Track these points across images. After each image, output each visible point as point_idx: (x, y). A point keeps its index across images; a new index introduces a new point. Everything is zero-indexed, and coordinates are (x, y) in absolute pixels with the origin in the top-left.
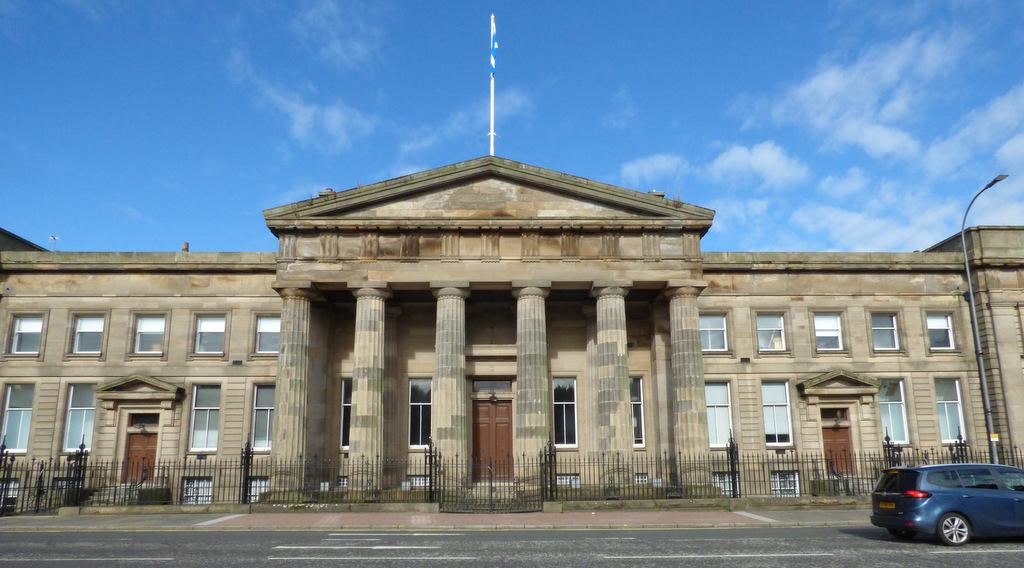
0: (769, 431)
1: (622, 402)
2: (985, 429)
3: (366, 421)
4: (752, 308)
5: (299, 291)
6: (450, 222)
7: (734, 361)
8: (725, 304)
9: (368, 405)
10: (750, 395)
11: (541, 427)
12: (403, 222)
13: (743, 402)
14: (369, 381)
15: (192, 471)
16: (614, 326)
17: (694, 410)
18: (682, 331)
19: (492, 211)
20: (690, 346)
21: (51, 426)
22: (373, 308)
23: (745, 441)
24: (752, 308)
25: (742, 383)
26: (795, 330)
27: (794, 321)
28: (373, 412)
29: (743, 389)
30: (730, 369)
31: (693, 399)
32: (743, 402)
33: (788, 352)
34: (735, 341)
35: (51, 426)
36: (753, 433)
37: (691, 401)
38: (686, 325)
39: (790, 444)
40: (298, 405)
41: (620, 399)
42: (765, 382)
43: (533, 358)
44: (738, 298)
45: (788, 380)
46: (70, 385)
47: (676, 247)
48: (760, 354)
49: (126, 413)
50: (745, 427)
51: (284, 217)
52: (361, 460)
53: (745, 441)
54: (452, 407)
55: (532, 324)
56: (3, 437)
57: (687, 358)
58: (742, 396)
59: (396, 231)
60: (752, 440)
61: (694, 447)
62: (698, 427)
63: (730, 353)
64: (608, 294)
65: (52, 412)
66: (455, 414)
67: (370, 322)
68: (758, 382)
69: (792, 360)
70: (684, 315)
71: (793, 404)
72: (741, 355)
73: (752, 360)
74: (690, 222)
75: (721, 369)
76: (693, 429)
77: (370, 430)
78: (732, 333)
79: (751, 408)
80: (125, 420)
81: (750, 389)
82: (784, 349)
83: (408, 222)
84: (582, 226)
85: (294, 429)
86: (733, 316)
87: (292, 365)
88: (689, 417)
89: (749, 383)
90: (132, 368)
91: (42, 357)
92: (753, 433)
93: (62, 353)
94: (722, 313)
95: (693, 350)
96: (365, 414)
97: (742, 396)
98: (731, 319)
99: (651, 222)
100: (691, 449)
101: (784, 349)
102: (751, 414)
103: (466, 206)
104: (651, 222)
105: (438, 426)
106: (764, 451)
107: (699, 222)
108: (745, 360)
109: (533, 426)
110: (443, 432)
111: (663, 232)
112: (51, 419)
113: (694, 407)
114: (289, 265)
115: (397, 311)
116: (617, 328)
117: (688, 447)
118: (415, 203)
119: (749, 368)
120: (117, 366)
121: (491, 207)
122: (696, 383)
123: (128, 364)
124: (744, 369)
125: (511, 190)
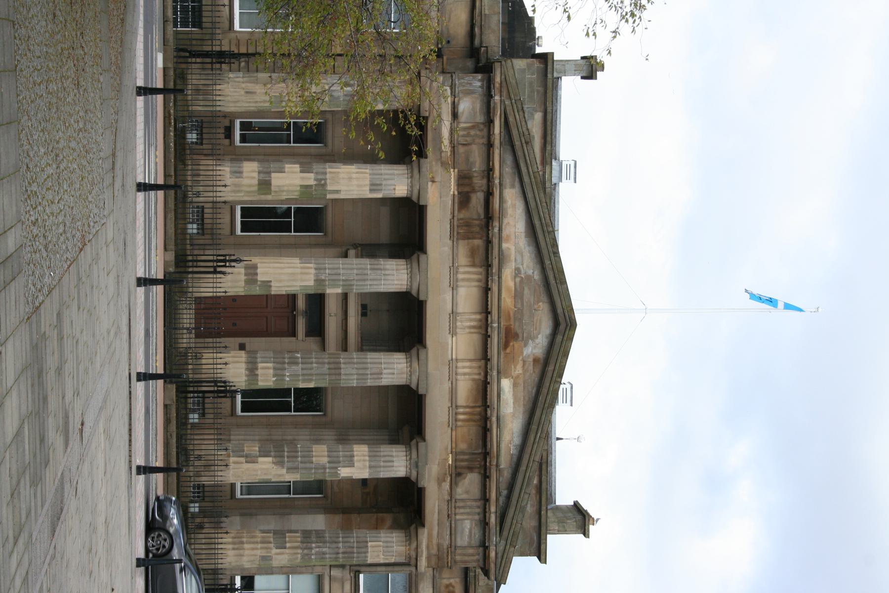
1: (284, 471)
14: (311, 186)
15: (209, 20)
16: (373, 464)
17: (275, 551)
18: (367, 542)
20: (349, 550)
31: (287, 551)
37: (285, 548)
38: (372, 547)
41: (288, 469)
47: (466, 538)
51: (504, 84)
57: (334, 545)
64: (410, 459)
85: (256, 102)
103: (518, 295)
105: (259, 265)
110: (252, 271)
113: (278, 551)
114: (448, 89)
118: (523, 235)
121: (517, 324)
122: (307, 555)
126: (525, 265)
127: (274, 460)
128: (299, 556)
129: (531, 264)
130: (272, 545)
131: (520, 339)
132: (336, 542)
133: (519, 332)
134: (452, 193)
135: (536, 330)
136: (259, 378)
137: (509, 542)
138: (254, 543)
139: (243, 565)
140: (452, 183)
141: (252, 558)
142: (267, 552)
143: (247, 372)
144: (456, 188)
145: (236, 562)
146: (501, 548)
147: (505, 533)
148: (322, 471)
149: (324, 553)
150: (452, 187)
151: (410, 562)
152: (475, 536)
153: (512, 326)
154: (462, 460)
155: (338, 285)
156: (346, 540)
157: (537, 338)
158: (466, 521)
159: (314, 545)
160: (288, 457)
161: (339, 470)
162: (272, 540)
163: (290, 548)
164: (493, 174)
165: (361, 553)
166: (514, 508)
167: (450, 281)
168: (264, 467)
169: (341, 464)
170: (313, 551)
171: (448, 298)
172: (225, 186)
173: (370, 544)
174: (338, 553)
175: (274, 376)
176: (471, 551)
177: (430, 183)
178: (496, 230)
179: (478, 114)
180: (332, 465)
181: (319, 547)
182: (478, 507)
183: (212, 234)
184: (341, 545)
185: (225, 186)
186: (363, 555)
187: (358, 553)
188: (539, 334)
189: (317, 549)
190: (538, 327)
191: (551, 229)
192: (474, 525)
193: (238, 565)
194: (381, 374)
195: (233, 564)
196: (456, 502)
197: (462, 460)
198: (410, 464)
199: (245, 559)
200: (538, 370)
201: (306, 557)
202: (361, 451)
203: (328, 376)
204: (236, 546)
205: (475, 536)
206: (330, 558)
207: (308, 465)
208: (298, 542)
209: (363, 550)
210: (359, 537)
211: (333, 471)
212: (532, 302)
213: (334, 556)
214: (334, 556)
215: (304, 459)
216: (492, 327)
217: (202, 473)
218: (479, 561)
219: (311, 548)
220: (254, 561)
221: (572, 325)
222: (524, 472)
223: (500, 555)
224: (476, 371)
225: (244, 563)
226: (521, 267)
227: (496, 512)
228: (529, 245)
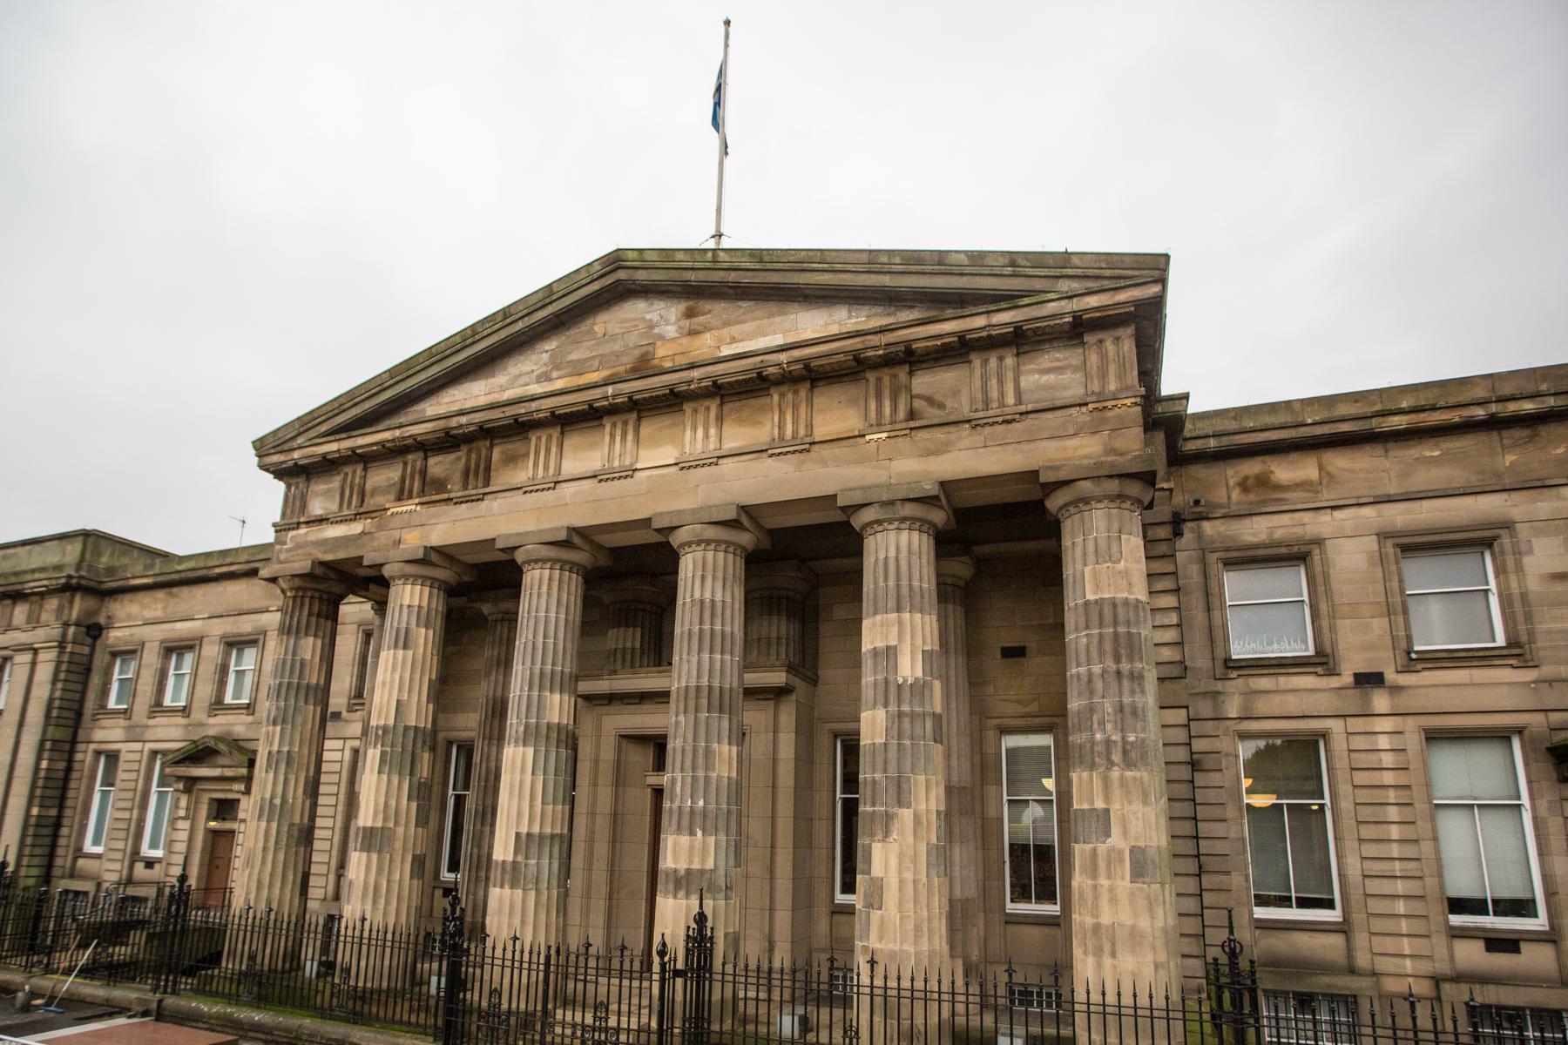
0: (1461, 884)
1: (906, 814)
2: (1075, 300)
3: (374, 840)
4: (1383, 536)
5: (296, 580)
6: (534, 405)
7: (1334, 682)
8: (1299, 530)
9: (376, 804)
10: (1388, 778)
11: (702, 872)
12: (454, 422)
13: (1364, 795)
14: (383, 754)
16: (891, 604)
17: (1116, 840)
18: (1087, 603)
19: (628, 361)
20: (1108, 647)
21: (126, 815)
22: (406, 602)
23: (1376, 906)
24: (1383, 536)
25: (1359, 743)
26: (1533, 585)
27: (1527, 561)
28: (386, 819)
29: (1363, 760)
30: (1323, 703)
31: (1115, 807)
32: (1364, 795)
33: (1517, 652)
34: (1333, 629)
35: (126, 815)
36: (1400, 887)
37: (1107, 811)
38: (1097, 587)
39: (1539, 923)
40: (278, 801)
41: (900, 804)
42: (1434, 737)
43: (692, 694)
44: (1338, 514)
45: (1520, 731)
46: (154, 753)
47: (1066, 377)
48: (1415, 661)
49: (205, 798)
50: (1375, 867)
51: (279, 448)
52: (358, 925)
53: (1374, 887)
54: (519, 814)
55: (696, 610)
56: (4, 845)
57: (1099, 685)
58: (1361, 778)
59: (447, 441)
60: (1401, 907)
61: (1113, 955)
62: (1132, 894)
63: (1322, 661)
64: (879, 522)
65: (130, 795)
66: (524, 830)
67: (398, 631)
68: (1413, 741)
69: (1530, 675)
70: (1091, 558)
71: (1543, 804)
72: (1352, 663)
73: (1391, 676)
74: (1093, 301)
75: (1292, 704)
76: (1113, 900)
77: (374, 856)
78: (1323, 607)
79: (1393, 813)
80: (204, 810)
81: (1395, 832)
82: (1311, 652)
83: (464, 420)
84: (806, 363)
85: (265, 849)
86: (1325, 562)
87: (275, 723)
88: (1102, 864)
89: (1383, 742)
90: (217, 725)
91: (252, 708)
92: (1400, 887)
93: (207, 704)
94: (1295, 555)
95: (1117, 659)
96: (369, 824)
97: (1361, 778)
98: (1318, 569)
99: (980, 322)
100: (1107, 961)
101: (1311, 652)
102: (1395, 832)
104: (980, 322)
106: (1440, 943)
107: (1122, 296)
108: (1369, 680)
109: (682, 866)
111: (1021, 340)
112: (128, 804)
113: (1115, 830)
115: (961, 568)
116: (899, 609)
117: (1098, 952)
118: (491, 381)
119: (1380, 701)
120: (201, 725)
122: (1125, 752)
123: (212, 721)
124: (1367, 701)
125: (664, 317)
126: (534, 368)
127: (880, 837)
128: (1129, 774)
129: (534, 358)
130: (1102, 848)
131: (651, 348)
132: (1090, 681)
133: (637, 352)
134: (418, 508)
135: (637, 326)
136: (696, 866)
137: (1057, 272)
138: (1096, 897)
139: (1165, 930)
140: (404, 509)
141: (1142, 903)
142: (1121, 861)
143: (681, 894)
144: (405, 503)
145: (1154, 948)
146: (1076, 286)
147: (1038, 285)
148: (906, 721)
149: (1121, 709)
150: (409, 508)
151: (213, 837)
152: (1058, 360)
153: (628, 366)
154: (879, 412)
155: (502, 702)
156: (1083, 657)
157: (651, 320)
158: (1023, 384)
159: (1098, 736)
160: (874, 804)
161: (905, 681)
162: (1088, 847)
163: (1107, 799)
164: (388, 441)
165: (1115, 615)
166: (977, 279)
167: (613, 479)
168: (894, 863)
169: (891, 678)
170: (1116, 737)
171: (572, 490)
172: (363, 920)
173: (1090, 597)
174: (1118, 673)
175: (692, 833)
176: (1093, 358)
177: (401, 546)
178: (464, 420)
179: (330, 486)
180: (892, 698)
181: (1102, 723)
182: (985, 362)
183: (363, 999)
184: (1097, 669)
185: (363, 920)
186: (1121, 611)
187: (1115, 623)
188: (643, 319)
189: (1109, 726)
190: (632, 324)
191: (469, 331)
192: (1032, 366)
193: (1167, 943)
194: (702, 602)
195: (1162, 957)
196: (976, 411)
197: (879, 412)
198: (890, 521)
199: (1144, 923)
200: (1544, 430)
201: (1133, 755)
202: (875, 632)
203: (699, 714)
204: (1107, 947)
205: (1058, 360)
206: (1133, 692)
207: (893, 754)
208: (1091, 777)
209: (1107, 611)
210: (1076, 625)
211: (906, 695)
212: (593, 342)
213: (1126, 683)
214: (1126, 683)
215: (880, 766)
216: (614, 396)
217: (906, 1023)
218: (1117, 339)
219: (1108, 743)
220: (1148, 898)
221: (615, 260)
222: (894, 276)
223: (1092, 285)
224: (701, 417)
225: (1160, 923)
226: (535, 374)
227: (988, 312)
228: (506, 369)
